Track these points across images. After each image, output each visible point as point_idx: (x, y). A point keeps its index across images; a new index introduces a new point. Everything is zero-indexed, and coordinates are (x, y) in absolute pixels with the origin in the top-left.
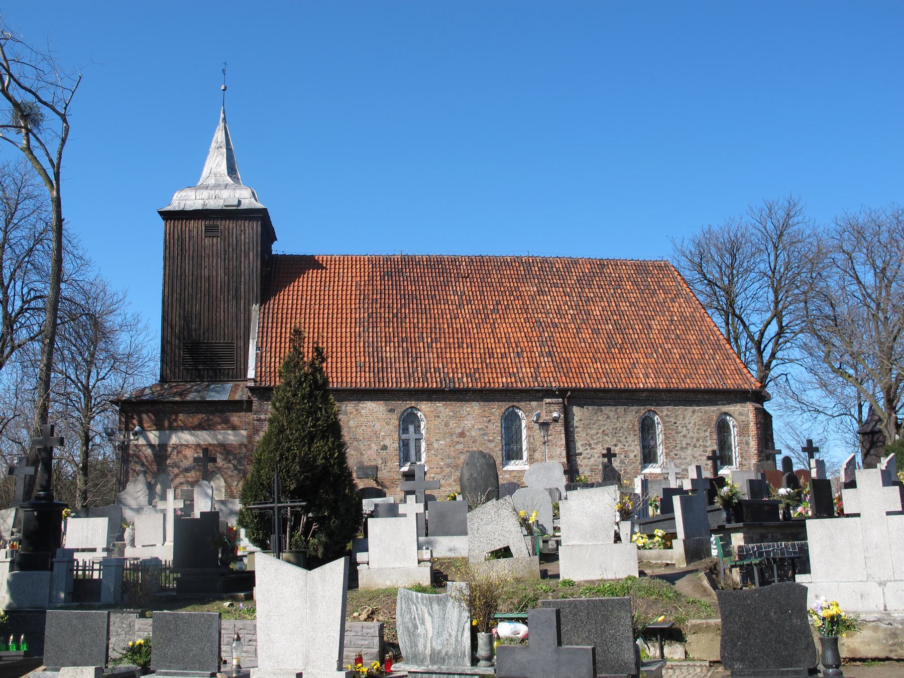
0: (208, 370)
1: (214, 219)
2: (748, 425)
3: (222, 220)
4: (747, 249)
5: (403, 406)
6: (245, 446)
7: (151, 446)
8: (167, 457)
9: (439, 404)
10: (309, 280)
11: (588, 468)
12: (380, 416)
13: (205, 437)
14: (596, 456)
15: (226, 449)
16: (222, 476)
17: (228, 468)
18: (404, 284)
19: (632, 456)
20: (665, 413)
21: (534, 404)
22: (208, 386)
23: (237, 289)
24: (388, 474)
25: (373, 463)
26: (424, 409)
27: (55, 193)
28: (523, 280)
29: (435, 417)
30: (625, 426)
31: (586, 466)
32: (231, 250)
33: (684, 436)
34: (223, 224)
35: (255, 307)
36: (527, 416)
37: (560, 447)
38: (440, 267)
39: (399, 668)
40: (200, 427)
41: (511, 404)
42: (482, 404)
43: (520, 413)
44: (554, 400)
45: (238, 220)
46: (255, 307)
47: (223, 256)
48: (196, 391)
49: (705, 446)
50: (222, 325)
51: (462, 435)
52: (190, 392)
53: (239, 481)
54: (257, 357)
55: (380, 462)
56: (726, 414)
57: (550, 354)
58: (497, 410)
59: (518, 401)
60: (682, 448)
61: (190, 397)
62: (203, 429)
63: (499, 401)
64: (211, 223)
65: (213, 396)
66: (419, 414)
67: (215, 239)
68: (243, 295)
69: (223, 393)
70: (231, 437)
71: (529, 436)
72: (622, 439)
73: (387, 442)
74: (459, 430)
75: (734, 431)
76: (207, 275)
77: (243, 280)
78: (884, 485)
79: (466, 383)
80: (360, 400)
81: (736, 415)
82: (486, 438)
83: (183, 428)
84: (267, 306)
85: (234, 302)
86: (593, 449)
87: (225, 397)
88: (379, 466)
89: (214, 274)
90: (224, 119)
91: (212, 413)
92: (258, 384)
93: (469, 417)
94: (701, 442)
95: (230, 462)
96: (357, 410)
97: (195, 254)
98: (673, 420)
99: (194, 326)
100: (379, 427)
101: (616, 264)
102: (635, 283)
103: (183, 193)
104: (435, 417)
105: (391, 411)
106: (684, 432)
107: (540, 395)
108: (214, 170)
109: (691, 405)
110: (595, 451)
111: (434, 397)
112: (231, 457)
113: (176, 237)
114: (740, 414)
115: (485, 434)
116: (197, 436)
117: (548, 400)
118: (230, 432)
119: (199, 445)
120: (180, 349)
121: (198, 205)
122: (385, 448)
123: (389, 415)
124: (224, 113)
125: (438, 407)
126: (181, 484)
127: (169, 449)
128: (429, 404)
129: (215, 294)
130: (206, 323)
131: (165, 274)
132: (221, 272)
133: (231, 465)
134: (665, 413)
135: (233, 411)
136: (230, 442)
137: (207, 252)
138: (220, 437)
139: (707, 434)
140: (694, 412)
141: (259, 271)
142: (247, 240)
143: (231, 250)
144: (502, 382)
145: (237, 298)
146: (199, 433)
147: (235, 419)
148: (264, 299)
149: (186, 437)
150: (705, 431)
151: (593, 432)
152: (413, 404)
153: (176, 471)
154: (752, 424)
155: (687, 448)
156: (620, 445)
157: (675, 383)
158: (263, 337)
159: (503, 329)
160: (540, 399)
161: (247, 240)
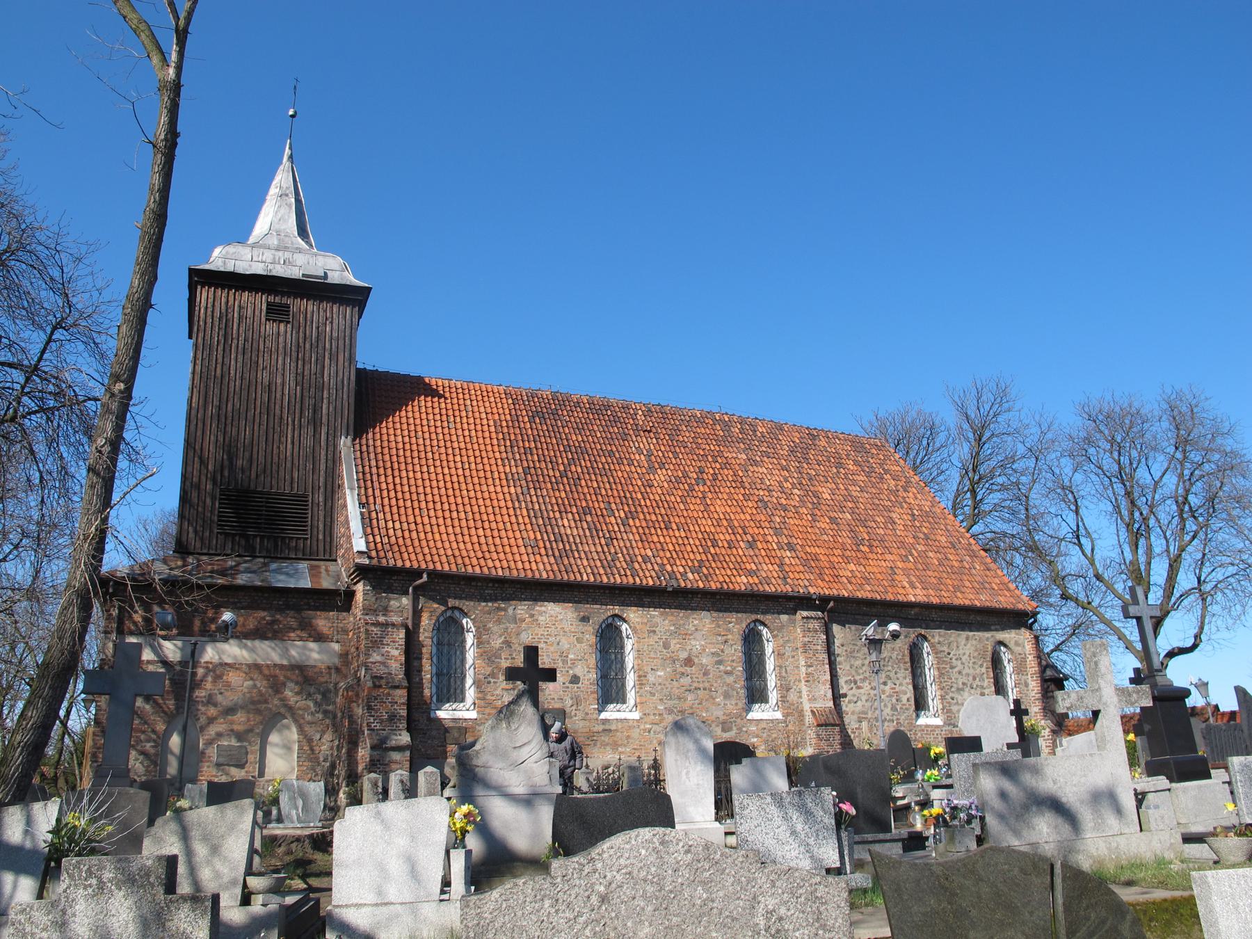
0: (262, 538)
1: (283, 294)
2: (1024, 659)
3: (295, 297)
4: (941, 439)
5: (602, 612)
6: (338, 670)
7: (165, 663)
8: (196, 685)
9: (655, 613)
10: (418, 411)
11: (855, 717)
12: (567, 627)
13: (268, 652)
14: (864, 698)
15: (304, 675)
16: (296, 721)
17: (306, 709)
18: (560, 435)
19: (904, 700)
20: (937, 639)
21: (784, 617)
22: (265, 565)
23: (316, 410)
24: (581, 724)
25: (557, 706)
26: (634, 619)
27: (171, 71)
28: (727, 440)
29: (650, 632)
30: (894, 656)
31: (853, 713)
32: (308, 346)
33: (960, 673)
34: (299, 305)
35: (344, 443)
36: (774, 637)
37: (824, 684)
38: (604, 412)
39: (23, 889)
40: (259, 634)
41: (754, 617)
42: (715, 614)
43: (765, 631)
44: (812, 614)
45: (321, 301)
46: (344, 443)
47: (294, 355)
48: (248, 571)
49: (982, 687)
50: (289, 465)
51: (689, 662)
52: (239, 572)
53: (323, 733)
54: (363, 518)
55: (569, 702)
56: (1001, 643)
57: (791, 547)
58: (736, 624)
59: (764, 613)
60: (959, 690)
61: (242, 579)
62: (263, 637)
63: (737, 612)
64: (277, 299)
65: (281, 581)
66: (624, 627)
67: (282, 326)
68: (324, 420)
69: (300, 577)
70: (314, 654)
71: (779, 667)
72: (892, 674)
73: (579, 670)
74: (683, 655)
75: (1009, 668)
76: (266, 381)
77: (325, 395)
78: (979, 738)
79: (693, 580)
80: (535, 600)
81: (1011, 645)
82: (722, 667)
83: (226, 632)
84: (364, 441)
85: (311, 432)
86: (859, 688)
87: (306, 583)
88: (568, 710)
89: (279, 381)
90: (291, 157)
91: (280, 610)
92: (375, 562)
93: (698, 635)
94: (977, 682)
95: (309, 695)
96: (532, 616)
97: (248, 346)
98: (945, 648)
99: (240, 462)
100: (567, 646)
101: (830, 436)
102: (856, 463)
103: (231, 249)
104: (650, 632)
105: (585, 619)
106: (960, 667)
107: (791, 605)
108: (275, 226)
109: (963, 630)
110: (862, 691)
111: (647, 600)
112: (312, 690)
113: (217, 314)
114: (1017, 644)
115: (720, 662)
116: (252, 650)
117: (805, 614)
118: (312, 645)
119: (256, 667)
120: (213, 498)
121: (258, 269)
122: (575, 680)
123: (582, 627)
124: (290, 148)
125: (653, 617)
126: (219, 735)
127: (200, 671)
128: (640, 611)
129: (278, 412)
130: (262, 459)
131: (194, 373)
132: (290, 378)
133: (311, 704)
134: (937, 639)
135: (317, 609)
136: (311, 663)
137: (268, 344)
138: (293, 653)
139: (984, 670)
140: (967, 639)
141: (353, 384)
142: (335, 335)
143: (308, 346)
144: (742, 583)
145: (315, 422)
146: (257, 643)
147: (323, 622)
148: (360, 428)
149: (232, 651)
150: (981, 666)
151: (858, 663)
152: (617, 610)
153: (212, 711)
154: (1031, 658)
155: (962, 690)
156: (890, 684)
157: (947, 598)
158: (366, 489)
159: (719, 508)
160: (793, 612)
161: (335, 335)
